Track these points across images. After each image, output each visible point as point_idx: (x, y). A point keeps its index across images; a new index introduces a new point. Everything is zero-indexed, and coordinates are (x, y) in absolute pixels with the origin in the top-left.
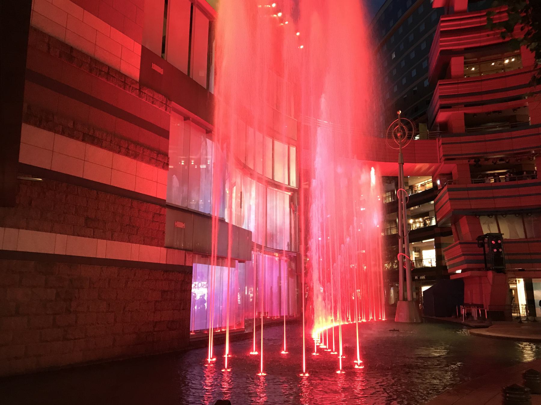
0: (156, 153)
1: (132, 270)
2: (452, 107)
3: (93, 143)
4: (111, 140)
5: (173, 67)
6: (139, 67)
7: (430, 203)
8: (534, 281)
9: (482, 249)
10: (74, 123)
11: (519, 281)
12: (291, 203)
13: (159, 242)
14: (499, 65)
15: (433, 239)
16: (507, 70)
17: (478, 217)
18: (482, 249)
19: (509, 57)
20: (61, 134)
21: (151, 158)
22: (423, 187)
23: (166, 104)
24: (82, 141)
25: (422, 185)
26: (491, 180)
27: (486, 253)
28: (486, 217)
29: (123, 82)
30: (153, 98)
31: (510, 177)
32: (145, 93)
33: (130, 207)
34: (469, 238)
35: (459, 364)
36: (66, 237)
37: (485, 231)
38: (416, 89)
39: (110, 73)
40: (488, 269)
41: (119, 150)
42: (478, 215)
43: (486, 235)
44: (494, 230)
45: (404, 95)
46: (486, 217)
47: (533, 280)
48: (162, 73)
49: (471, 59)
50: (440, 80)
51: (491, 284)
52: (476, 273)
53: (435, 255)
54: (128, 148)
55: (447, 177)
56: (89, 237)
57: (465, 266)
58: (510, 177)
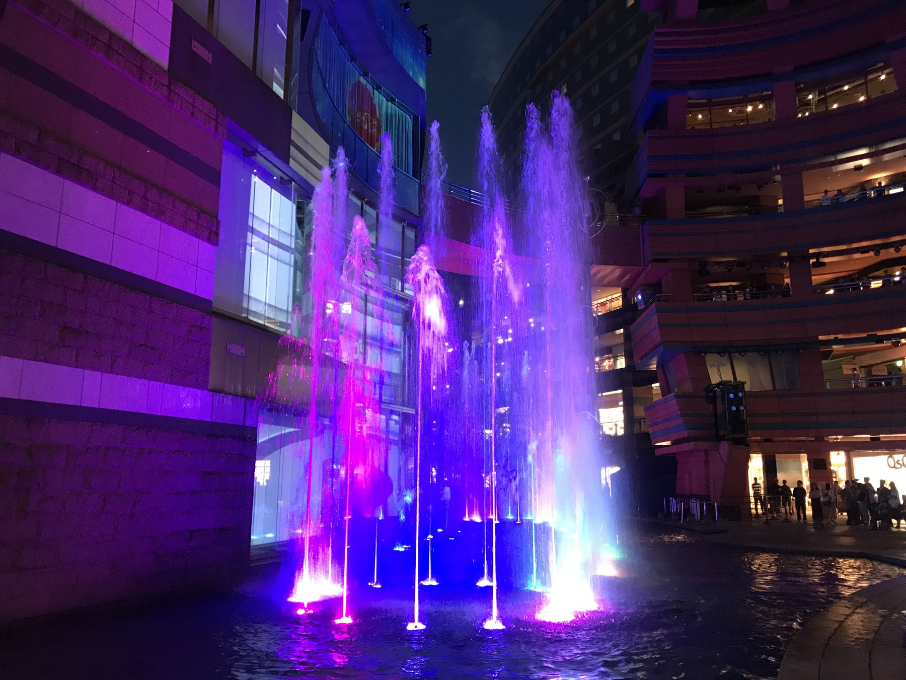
0: (196, 211)
1: (148, 431)
3: (77, 180)
4: (114, 178)
5: (229, 54)
6: (168, 43)
7: (615, 333)
8: (779, 458)
10: (39, 136)
12: (406, 323)
13: (199, 380)
15: (620, 391)
17: (703, 354)
18: (712, 405)
19: (752, 101)
20: (14, 155)
21: (187, 220)
22: (603, 307)
23: (216, 121)
24: (57, 172)
25: (603, 304)
26: (723, 296)
27: (719, 413)
28: (716, 356)
29: (137, 67)
30: (193, 106)
31: (751, 292)
32: (179, 95)
33: (148, 310)
34: (688, 387)
36: (21, 363)
37: (715, 380)
39: (113, 46)
40: (720, 439)
41: (129, 198)
42: (703, 352)
43: (718, 385)
44: (728, 377)
47: (777, 455)
48: (210, 61)
51: (725, 462)
52: (703, 445)
54: (145, 196)
55: (654, 289)
56: (67, 365)
57: (676, 436)
58: (751, 292)
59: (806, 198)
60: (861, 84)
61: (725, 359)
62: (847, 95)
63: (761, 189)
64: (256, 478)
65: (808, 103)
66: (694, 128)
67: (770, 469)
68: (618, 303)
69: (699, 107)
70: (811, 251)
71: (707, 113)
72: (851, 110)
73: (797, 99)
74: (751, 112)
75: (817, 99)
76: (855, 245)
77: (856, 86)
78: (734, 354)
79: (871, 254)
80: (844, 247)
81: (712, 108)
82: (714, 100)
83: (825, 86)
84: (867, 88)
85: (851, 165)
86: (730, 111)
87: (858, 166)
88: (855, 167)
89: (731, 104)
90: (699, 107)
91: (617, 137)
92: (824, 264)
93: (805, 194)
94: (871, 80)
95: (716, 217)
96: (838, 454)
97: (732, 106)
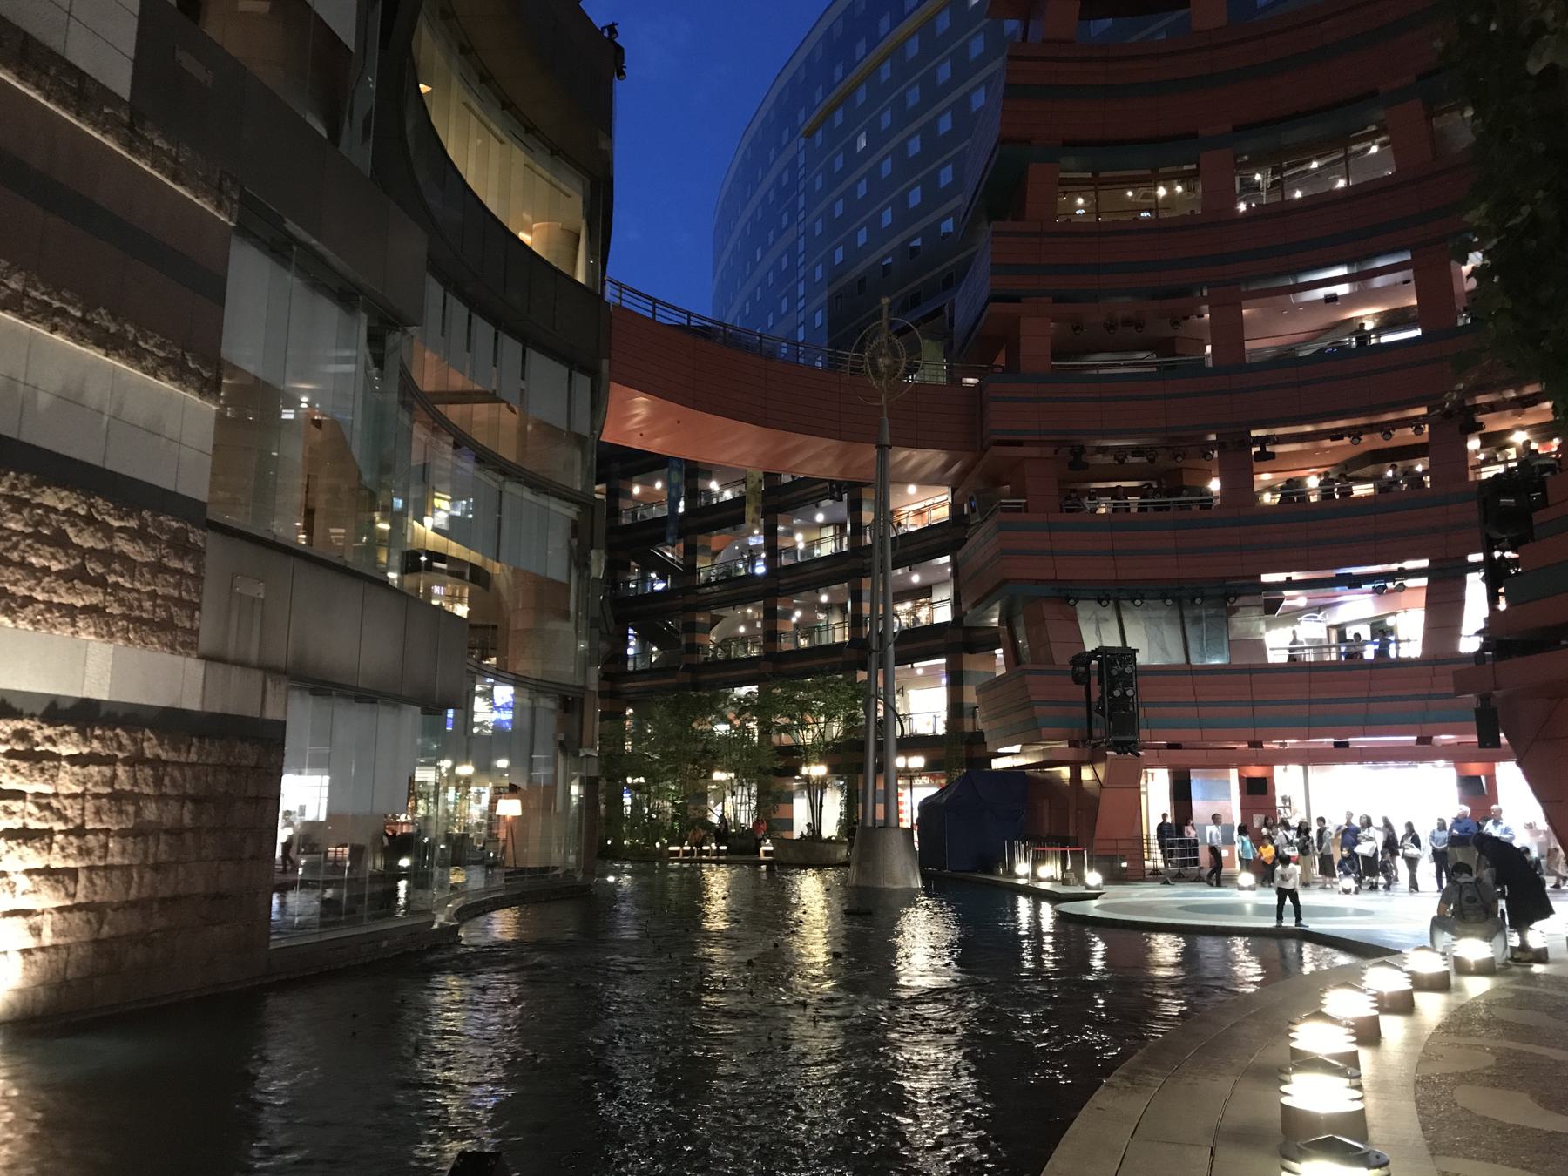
2: (1022, 300)
9: (1082, 688)
11: (1153, 774)
14: (1142, 198)
15: (943, 661)
16: (1164, 215)
18: (1082, 688)
19: (1167, 180)
25: (919, 513)
35: (751, 1026)
37: (1090, 646)
38: (917, 242)
44: (1113, 641)
45: (885, 257)
46: (1094, 603)
49: (1072, 172)
50: (994, 222)
53: (945, 706)
59: (1248, 345)
60: (1339, 160)
61: (1108, 612)
62: (1318, 176)
63: (1176, 327)
64: (1416, 767)
65: (1256, 187)
66: (1069, 220)
67: (1181, 794)
68: (942, 513)
69: (1078, 186)
70: (1254, 434)
71: (1092, 195)
72: (1323, 203)
73: (1237, 179)
74: (1165, 198)
75: (1269, 180)
76: (1326, 426)
77: (1333, 162)
78: (1124, 602)
79: (1347, 440)
80: (1309, 428)
81: (1099, 187)
82: (1103, 175)
83: (1281, 159)
84: (1347, 166)
85: (1321, 293)
86: (1130, 194)
87: (1331, 295)
88: (1326, 296)
89: (1132, 182)
90: (1078, 185)
91: (948, 226)
92: (1272, 456)
93: (1246, 337)
94: (1357, 153)
95: (1101, 372)
96: (1285, 770)
97: (1133, 185)
